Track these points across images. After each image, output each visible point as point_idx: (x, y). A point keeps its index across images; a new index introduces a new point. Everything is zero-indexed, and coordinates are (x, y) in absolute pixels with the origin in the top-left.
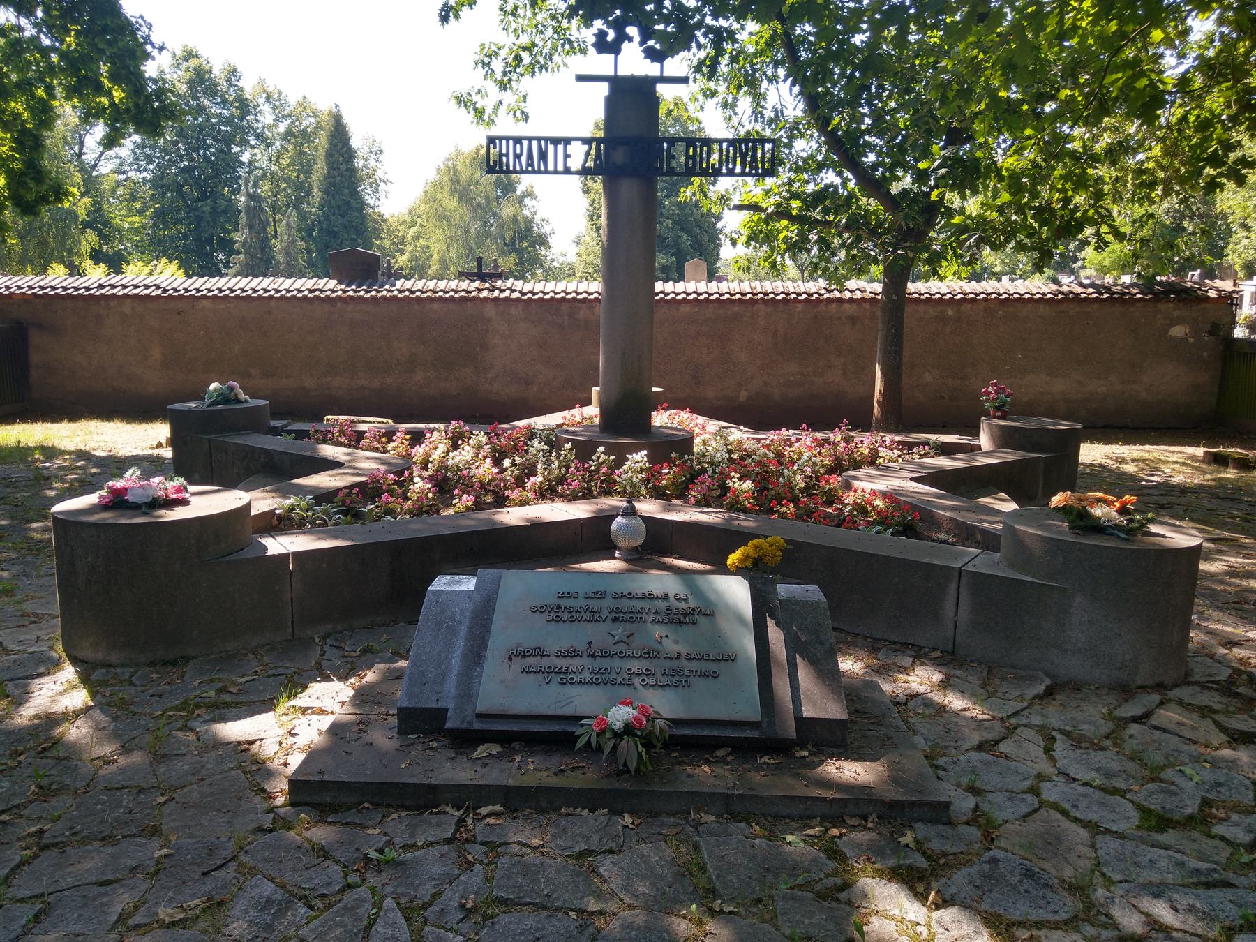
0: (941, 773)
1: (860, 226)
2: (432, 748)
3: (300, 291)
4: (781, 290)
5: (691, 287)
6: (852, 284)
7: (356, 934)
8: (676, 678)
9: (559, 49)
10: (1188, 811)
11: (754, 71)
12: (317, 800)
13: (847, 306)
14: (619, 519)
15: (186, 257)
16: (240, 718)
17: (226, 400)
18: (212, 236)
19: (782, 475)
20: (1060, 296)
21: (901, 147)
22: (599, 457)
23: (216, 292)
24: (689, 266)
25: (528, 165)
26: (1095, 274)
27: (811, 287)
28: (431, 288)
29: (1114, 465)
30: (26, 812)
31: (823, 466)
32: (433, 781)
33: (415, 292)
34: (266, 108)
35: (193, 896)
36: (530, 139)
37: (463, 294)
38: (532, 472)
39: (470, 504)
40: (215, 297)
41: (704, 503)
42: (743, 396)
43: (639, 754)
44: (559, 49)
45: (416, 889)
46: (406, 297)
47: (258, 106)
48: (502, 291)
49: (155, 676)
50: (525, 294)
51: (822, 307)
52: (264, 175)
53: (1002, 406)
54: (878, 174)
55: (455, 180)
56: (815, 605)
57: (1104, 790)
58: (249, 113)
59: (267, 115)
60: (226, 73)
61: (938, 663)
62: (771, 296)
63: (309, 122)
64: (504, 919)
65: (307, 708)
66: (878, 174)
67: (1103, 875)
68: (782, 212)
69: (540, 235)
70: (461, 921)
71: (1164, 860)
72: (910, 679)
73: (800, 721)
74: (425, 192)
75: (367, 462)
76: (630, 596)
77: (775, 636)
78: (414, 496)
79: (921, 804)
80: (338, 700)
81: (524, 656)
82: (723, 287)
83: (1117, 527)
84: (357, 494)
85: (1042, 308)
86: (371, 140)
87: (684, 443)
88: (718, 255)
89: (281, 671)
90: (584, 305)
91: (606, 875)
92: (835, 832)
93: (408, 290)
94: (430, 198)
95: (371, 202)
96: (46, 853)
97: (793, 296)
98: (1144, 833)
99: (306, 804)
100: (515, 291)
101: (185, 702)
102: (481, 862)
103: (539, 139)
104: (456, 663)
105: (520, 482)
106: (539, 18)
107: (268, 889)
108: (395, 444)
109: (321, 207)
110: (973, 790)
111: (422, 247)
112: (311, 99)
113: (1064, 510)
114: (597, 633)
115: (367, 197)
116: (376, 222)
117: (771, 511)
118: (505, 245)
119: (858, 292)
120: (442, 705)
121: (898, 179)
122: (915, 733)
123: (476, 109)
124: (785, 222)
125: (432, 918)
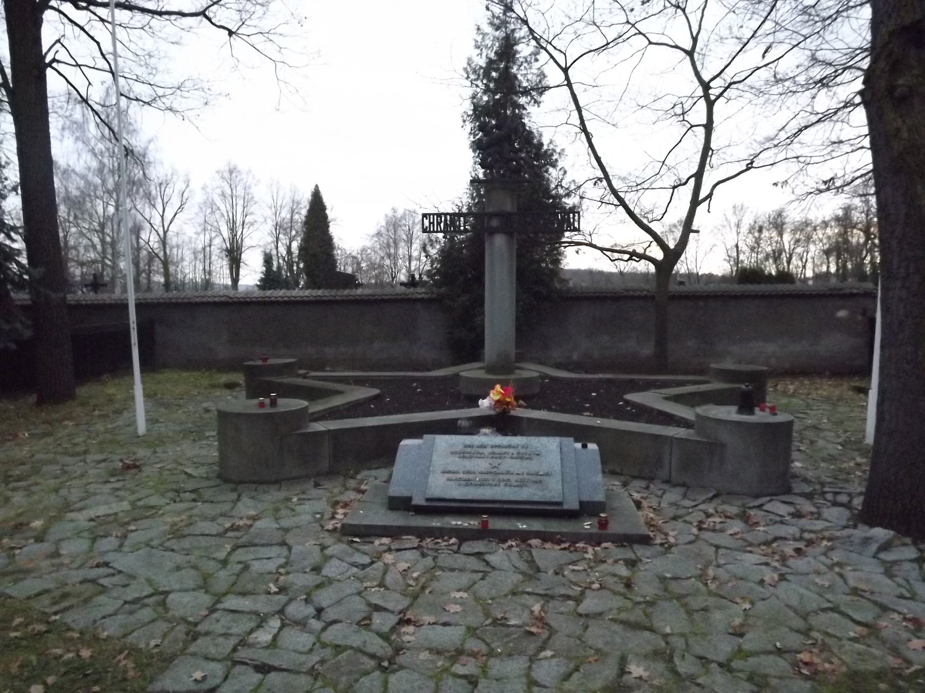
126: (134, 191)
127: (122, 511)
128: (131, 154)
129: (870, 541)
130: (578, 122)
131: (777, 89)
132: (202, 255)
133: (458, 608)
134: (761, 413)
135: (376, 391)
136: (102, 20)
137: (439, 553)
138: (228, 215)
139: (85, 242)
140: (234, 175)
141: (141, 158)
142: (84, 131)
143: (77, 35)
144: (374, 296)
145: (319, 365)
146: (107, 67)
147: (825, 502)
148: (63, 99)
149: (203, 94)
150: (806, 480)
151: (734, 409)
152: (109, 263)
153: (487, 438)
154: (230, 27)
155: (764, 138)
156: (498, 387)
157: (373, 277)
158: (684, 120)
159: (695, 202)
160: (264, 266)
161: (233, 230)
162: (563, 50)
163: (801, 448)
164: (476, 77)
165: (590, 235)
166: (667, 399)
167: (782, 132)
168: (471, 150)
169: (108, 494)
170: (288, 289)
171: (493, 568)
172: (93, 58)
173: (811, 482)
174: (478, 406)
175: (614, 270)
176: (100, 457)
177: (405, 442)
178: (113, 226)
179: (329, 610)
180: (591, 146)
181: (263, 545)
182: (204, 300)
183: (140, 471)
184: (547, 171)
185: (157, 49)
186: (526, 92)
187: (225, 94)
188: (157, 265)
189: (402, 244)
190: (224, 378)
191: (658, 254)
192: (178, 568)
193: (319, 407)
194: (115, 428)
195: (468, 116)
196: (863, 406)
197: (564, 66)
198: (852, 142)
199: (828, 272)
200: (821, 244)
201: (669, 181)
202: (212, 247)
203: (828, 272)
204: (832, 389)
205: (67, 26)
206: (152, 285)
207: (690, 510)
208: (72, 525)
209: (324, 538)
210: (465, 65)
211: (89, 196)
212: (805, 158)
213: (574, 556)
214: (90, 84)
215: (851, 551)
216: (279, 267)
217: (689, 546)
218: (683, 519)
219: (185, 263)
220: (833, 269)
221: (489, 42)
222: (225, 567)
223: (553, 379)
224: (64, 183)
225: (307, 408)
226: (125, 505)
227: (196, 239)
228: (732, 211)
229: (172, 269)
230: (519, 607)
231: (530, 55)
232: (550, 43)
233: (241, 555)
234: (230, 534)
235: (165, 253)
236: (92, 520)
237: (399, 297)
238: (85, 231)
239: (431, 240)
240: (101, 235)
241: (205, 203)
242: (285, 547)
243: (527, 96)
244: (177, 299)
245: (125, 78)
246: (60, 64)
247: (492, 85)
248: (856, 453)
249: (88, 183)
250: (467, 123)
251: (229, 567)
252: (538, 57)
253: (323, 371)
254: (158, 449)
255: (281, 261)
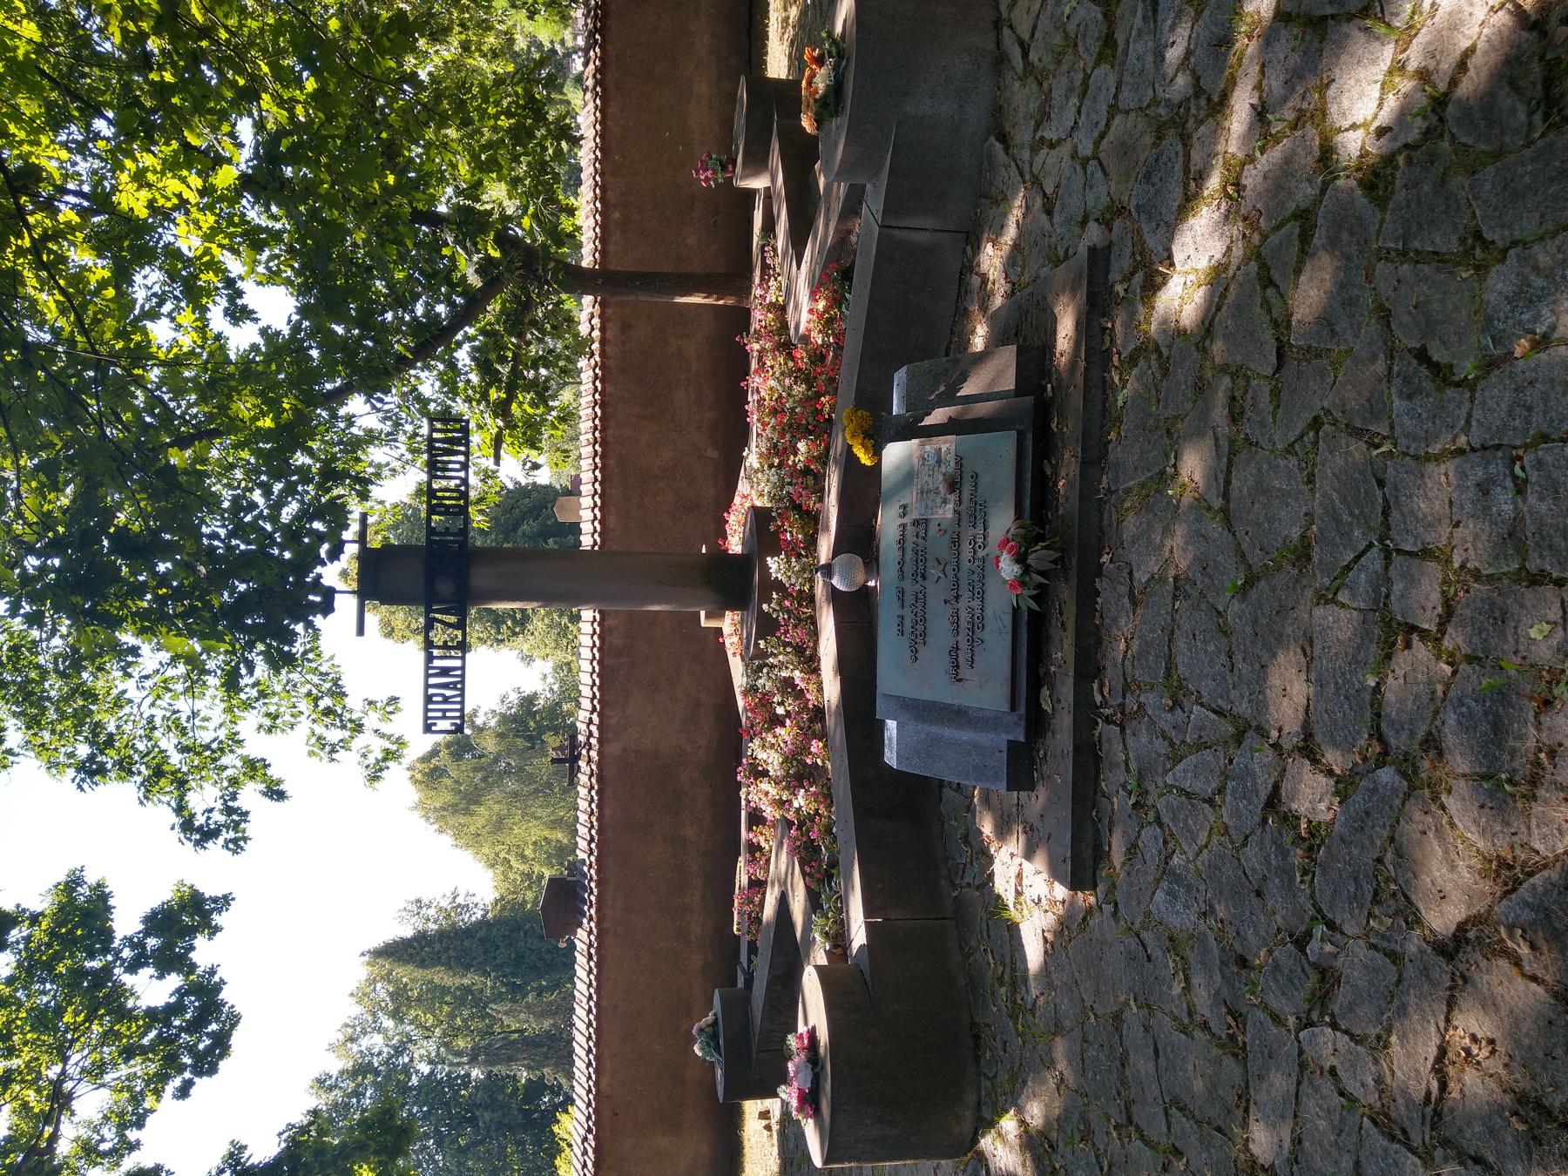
0: (1071, 252)
1: (518, 319)
2: (1045, 754)
3: (590, 972)
4: (590, 410)
5: (586, 515)
6: (584, 329)
7: (1193, 805)
8: (975, 513)
9: (314, 665)
10: (1099, 16)
11: (340, 442)
12: (1090, 862)
13: (609, 335)
14: (835, 582)
15: (546, 1142)
16: (1025, 956)
17: (715, 1036)
18: (521, 1110)
19: (793, 409)
20: (598, 89)
21: (428, 277)
22: (774, 610)
23: (591, 1070)
24: (562, 518)
25: (455, 688)
26: (570, 29)
27: (587, 376)
28: (586, 817)
29: (790, 32)
30: (1101, 1147)
31: (786, 364)
32: (1071, 749)
33: (591, 836)
34: (365, 1042)
35: (1166, 967)
36: (427, 686)
37: (594, 780)
38: (789, 682)
39: (821, 744)
40: (596, 1071)
41: (820, 492)
42: (713, 454)
43: (1043, 548)
44: (314, 665)
45: (1160, 755)
46: (597, 847)
47: (361, 1052)
48: (591, 734)
49: (988, 1054)
50: (594, 707)
51: (610, 363)
52: (446, 1045)
53: (721, 164)
54: (459, 300)
55: (454, 809)
56: (911, 377)
57: (1083, 94)
58: (370, 1063)
59: (372, 1041)
60: (321, 1092)
61: (977, 249)
62: (597, 421)
63: (382, 991)
64: (1182, 670)
65: (1016, 890)
66: (459, 300)
67: (1148, 106)
68: (502, 409)
69: (521, 705)
70: (1183, 709)
71: (1137, 48)
72: (991, 278)
73: (1020, 391)
74: (468, 846)
75: (781, 862)
76: (901, 563)
77: (938, 416)
78: (813, 806)
79: (1090, 276)
80: (1009, 862)
81: (958, 666)
82: (587, 477)
83: (836, 68)
84: (812, 867)
85: (613, 109)
86: (404, 914)
87: (760, 517)
88: (546, 487)
89: (984, 925)
90: (607, 638)
91: (1147, 576)
92: (1115, 359)
93: (589, 844)
94: (473, 841)
95: (479, 914)
96: (1135, 1118)
97: (597, 396)
98: (1117, 62)
99: (1094, 875)
100: (591, 719)
101: (1010, 1016)
102: (1139, 696)
103: (427, 676)
104: (965, 735)
105: (799, 695)
106: (278, 688)
107: (1160, 895)
108: (762, 839)
109: (486, 974)
110: (1084, 223)
111: (535, 851)
112: (353, 986)
113: (819, 121)
114: (936, 594)
115: (473, 919)
116: (503, 908)
117: (830, 420)
118: (532, 748)
119: (593, 322)
120: (1004, 747)
121: (464, 277)
122: (1037, 277)
123: (385, 759)
124: (514, 406)
125: (1181, 737)
225: (818, 968)
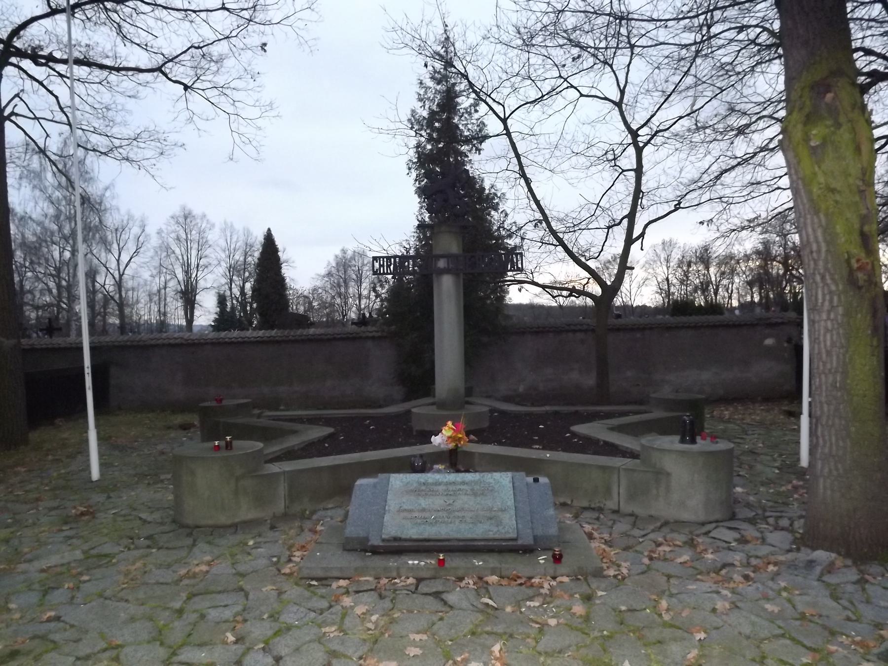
126: (90, 237)
127: (75, 560)
128: (87, 202)
129: (814, 564)
130: (517, 168)
131: (698, 137)
132: (158, 297)
133: (417, 651)
134: (703, 442)
135: (330, 430)
136: (61, 75)
137: (397, 594)
138: (183, 258)
139: (41, 286)
140: (188, 220)
141: (97, 206)
142: (41, 180)
143: (35, 89)
144: (326, 335)
145: (274, 404)
146: (64, 119)
147: (766, 526)
148: (21, 150)
149: (158, 144)
150: (748, 505)
151: (677, 438)
152: (64, 306)
153: (439, 476)
154: (185, 81)
155: (689, 181)
156: (450, 423)
157: (324, 315)
158: (615, 165)
159: (629, 241)
160: (218, 307)
161: (187, 272)
162: (501, 102)
163: (741, 473)
164: (420, 127)
165: (532, 273)
166: (612, 429)
167: (705, 175)
168: (416, 195)
169: (61, 542)
170: (242, 330)
171: (451, 607)
172: (52, 111)
173: (753, 506)
174: (431, 443)
175: (554, 304)
176: (55, 503)
177: (360, 482)
178: (69, 270)
179: (288, 658)
180: (530, 190)
181: (220, 592)
182: (160, 342)
183: (94, 517)
184: (489, 214)
185: (114, 102)
186: (467, 141)
187: (180, 144)
188: (113, 307)
189: (352, 283)
190: (179, 419)
191: (595, 289)
192: (133, 619)
193: (275, 448)
194: (68, 473)
195: (414, 163)
196: (795, 429)
197: (502, 116)
198: (768, 183)
199: (752, 302)
200: (744, 276)
201: (604, 222)
202: (167, 290)
203: (752, 302)
204: (764, 414)
205: (26, 80)
206: (107, 328)
207: (641, 540)
208: (22, 577)
209: (281, 582)
210: (410, 117)
211: (46, 241)
212: (727, 199)
213: (530, 592)
214: (48, 136)
215: (796, 575)
216: (233, 307)
217: (642, 577)
218: (634, 549)
219: (140, 305)
220: (757, 299)
221: (430, 95)
222: (180, 617)
223: (503, 413)
224: (21, 229)
226: (78, 554)
227: (151, 282)
228: (661, 247)
229: (127, 311)
230: (478, 648)
231: (470, 106)
232: (490, 96)
233: (200, 603)
234: (186, 582)
235: (121, 295)
236: (43, 571)
237: (351, 336)
238: (40, 276)
239: (380, 281)
240: (57, 280)
241: (160, 247)
242: (243, 593)
243: (468, 145)
244: (132, 342)
245: (83, 130)
246: (18, 117)
247: (435, 135)
248: (793, 476)
249: (45, 229)
250: (413, 170)
251: (185, 616)
252: (478, 108)
253: (277, 409)
254: (112, 495)
255: (235, 302)
